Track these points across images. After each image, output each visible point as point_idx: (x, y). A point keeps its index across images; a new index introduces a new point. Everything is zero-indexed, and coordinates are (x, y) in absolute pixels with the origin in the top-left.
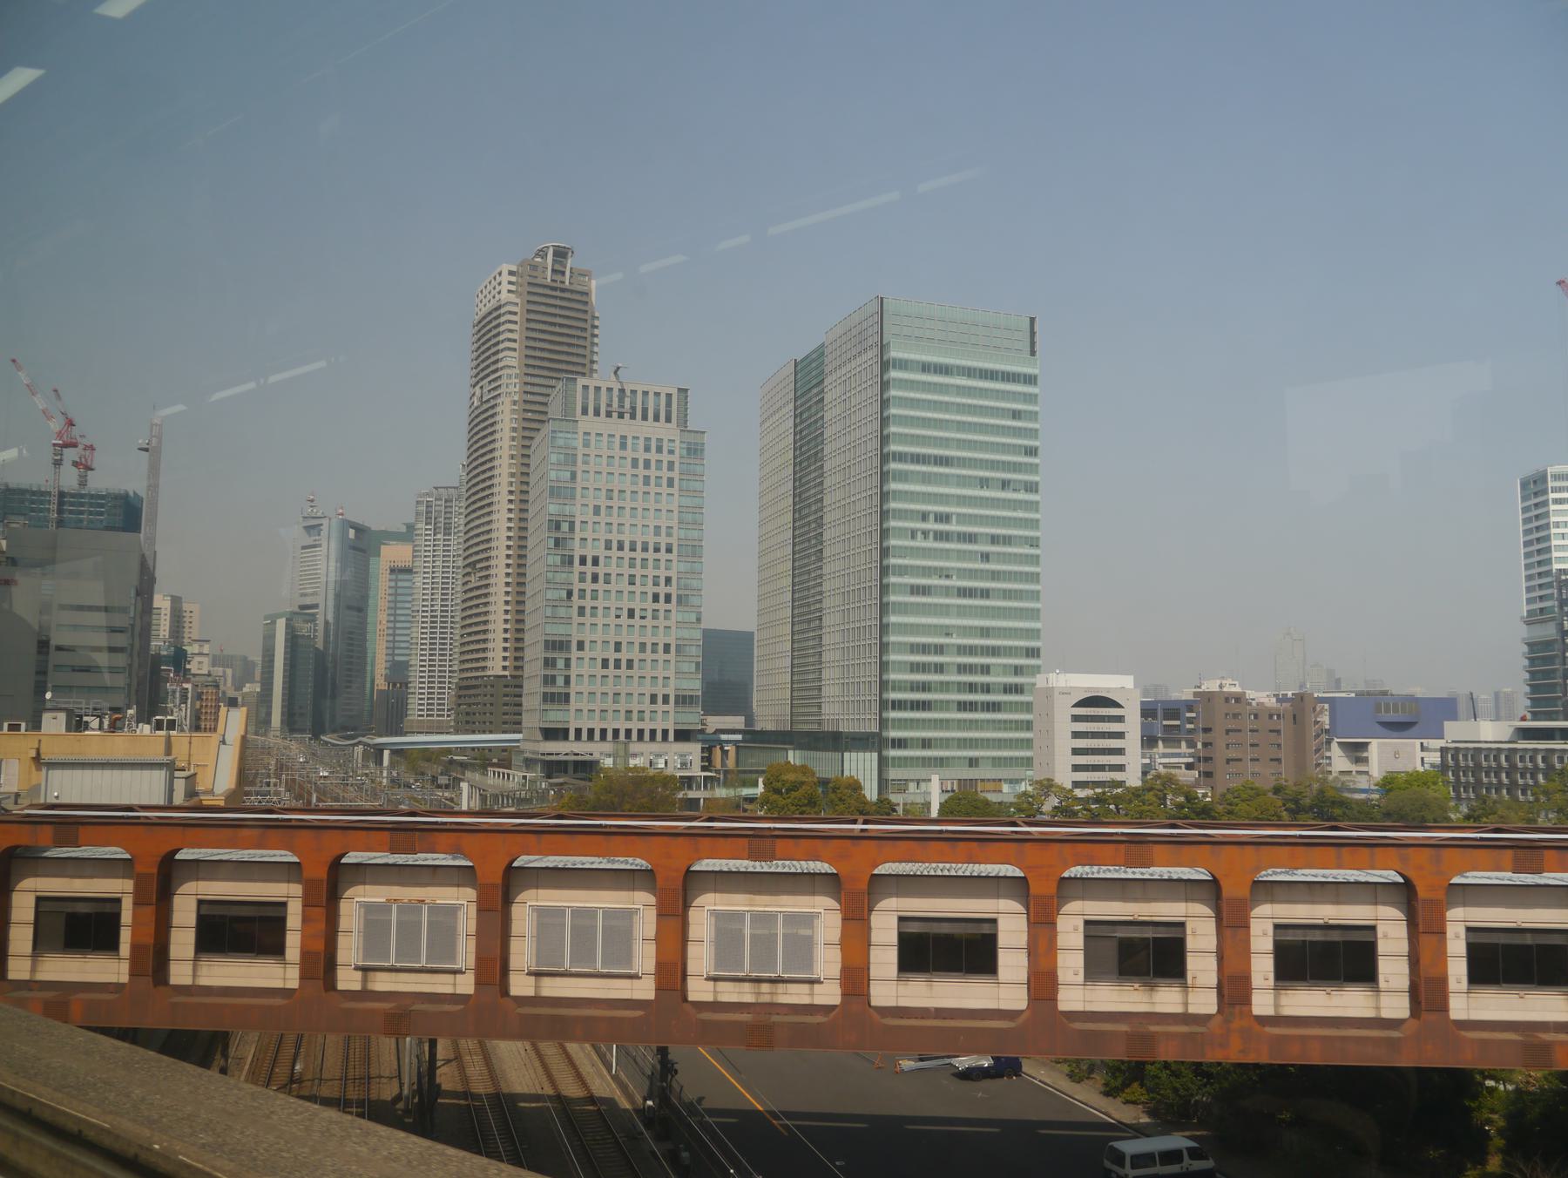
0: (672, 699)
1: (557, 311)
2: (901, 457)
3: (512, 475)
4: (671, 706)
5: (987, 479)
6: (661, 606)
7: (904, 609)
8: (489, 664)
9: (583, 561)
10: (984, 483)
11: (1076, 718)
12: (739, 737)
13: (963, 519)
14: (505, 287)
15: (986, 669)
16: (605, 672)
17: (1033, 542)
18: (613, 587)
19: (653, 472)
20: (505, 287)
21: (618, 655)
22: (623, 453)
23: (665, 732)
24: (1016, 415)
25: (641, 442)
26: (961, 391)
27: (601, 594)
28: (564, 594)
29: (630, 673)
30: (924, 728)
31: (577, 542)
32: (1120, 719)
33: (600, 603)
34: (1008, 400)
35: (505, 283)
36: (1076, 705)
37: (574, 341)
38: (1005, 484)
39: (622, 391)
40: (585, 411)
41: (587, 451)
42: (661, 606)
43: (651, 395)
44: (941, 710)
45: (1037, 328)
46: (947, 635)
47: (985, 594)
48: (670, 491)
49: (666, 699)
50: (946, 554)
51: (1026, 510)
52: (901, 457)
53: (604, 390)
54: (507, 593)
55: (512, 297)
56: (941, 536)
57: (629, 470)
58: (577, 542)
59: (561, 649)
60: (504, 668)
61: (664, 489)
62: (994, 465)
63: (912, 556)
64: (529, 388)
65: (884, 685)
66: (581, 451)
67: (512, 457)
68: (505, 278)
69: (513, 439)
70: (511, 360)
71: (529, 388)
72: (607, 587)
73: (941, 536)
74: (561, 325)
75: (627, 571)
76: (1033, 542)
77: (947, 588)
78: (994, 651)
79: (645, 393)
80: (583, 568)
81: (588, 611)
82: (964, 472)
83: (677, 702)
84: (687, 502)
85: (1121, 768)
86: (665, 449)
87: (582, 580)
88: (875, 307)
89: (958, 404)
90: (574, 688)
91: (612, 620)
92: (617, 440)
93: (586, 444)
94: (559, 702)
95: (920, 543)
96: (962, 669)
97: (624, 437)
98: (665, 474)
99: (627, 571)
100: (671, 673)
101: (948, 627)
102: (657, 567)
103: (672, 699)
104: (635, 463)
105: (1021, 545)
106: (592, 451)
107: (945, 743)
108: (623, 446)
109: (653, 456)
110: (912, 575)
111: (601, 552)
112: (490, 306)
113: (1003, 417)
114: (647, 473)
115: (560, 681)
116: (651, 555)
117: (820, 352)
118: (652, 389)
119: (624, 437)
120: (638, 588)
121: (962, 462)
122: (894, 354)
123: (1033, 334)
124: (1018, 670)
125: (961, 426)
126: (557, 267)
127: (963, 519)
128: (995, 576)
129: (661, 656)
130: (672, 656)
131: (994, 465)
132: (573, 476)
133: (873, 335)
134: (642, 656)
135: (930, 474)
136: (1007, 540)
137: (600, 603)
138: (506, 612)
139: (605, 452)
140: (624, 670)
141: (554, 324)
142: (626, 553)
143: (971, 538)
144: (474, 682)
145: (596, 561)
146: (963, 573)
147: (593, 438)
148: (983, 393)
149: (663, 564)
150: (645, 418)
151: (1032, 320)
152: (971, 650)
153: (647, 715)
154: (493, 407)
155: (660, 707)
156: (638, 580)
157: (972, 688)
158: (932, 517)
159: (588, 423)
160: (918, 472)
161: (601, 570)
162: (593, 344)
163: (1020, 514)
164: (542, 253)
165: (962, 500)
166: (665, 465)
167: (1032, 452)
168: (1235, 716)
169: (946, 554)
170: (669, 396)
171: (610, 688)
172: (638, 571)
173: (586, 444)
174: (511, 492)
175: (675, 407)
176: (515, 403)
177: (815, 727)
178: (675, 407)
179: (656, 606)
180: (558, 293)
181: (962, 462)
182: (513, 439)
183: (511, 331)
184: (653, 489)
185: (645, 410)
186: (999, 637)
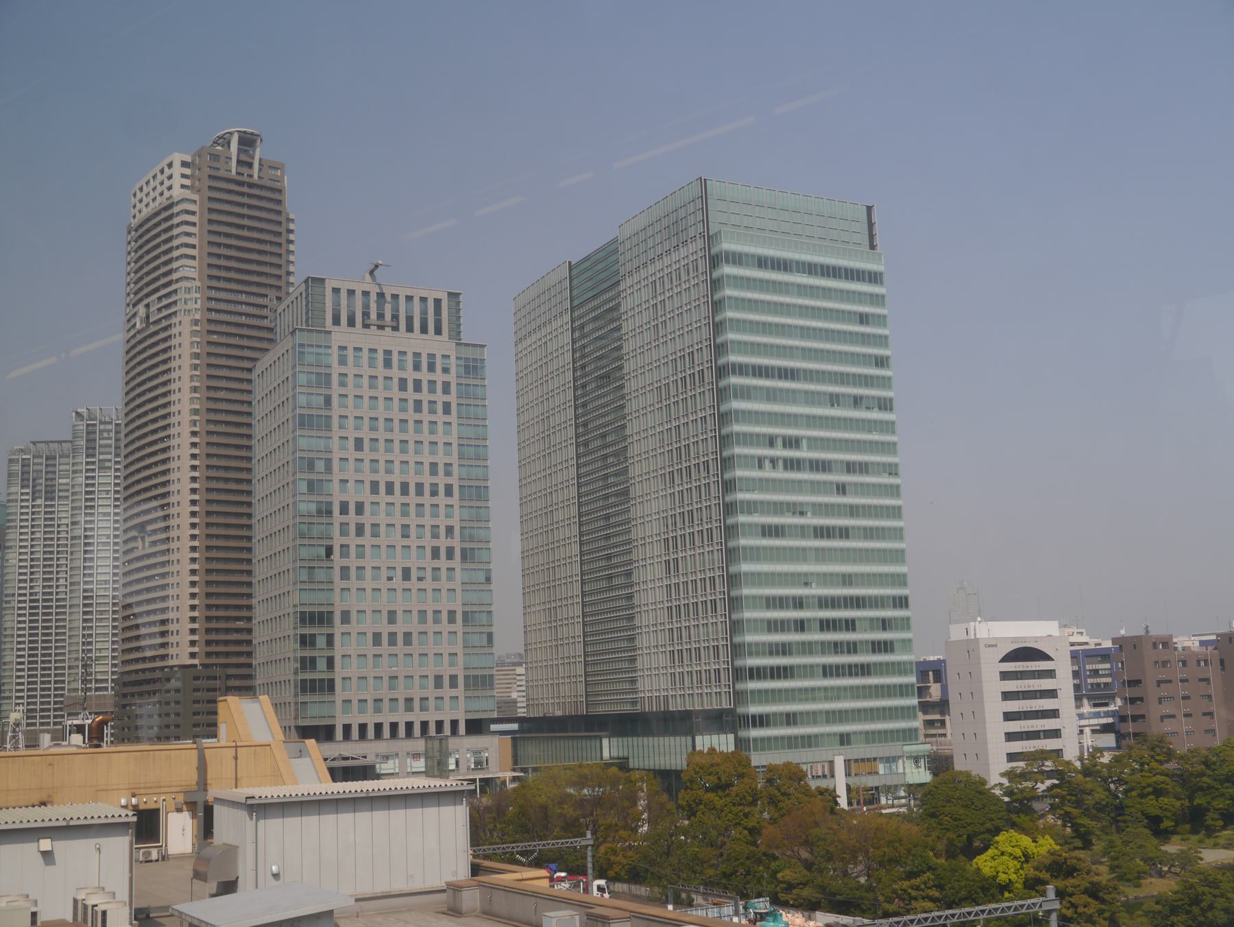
0: (461, 681)
1: (245, 211)
2: (741, 370)
3: (196, 412)
4: (460, 691)
5: (837, 395)
6: (443, 563)
7: (756, 554)
8: (171, 651)
9: (344, 509)
10: (834, 400)
11: (1005, 676)
12: (515, 726)
13: (814, 443)
14: (177, 181)
15: (850, 625)
16: (377, 650)
17: (892, 470)
18: (383, 541)
19: (425, 396)
20: (177, 181)
21: (392, 628)
22: (388, 373)
23: (454, 724)
24: (863, 319)
25: (410, 358)
26: (803, 290)
27: (368, 550)
28: (322, 552)
29: (408, 649)
30: (787, 700)
31: (336, 485)
32: (1050, 674)
33: (368, 562)
34: (854, 302)
35: (177, 177)
36: (1004, 660)
37: (267, 248)
38: (857, 401)
39: (381, 295)
40: (336, 321)
41: (343, 370)
42: (443, 563)
43: (416, 301)
44: (805, 676)
45: (875, 218)
46: (806, 584)
47: (844, 533)
48: (447, 418)
49: (453, 680)
50: (798, 486)
51: (881, 431)
52: (741, 370)
53: (358, 294)
54: (193, 560)
55: (188, 194)
56: (791, 464)
57: (396, 393)
58: (336, 485)
59: (321, 622)
60: (193, 655)
61: (440, 417)
62: (843, 379)
63: (761, 490)
64: (213, 305)
65: (737, 650)
66: (336, 370)
67: (195, 389)
68: (177, 170)
69: (195, 367)
70: (189, 272)
71: (213, 305)
72: (375, 541)
73: (791, 464)
74: (250, 228)
75: (398, 521)
76: (892, 470)
77: (802, 527)
78: (858, 602)
79: (409, 298)
80: (344, 518)
81: (353, 573)
82: (812, 387)
83: (467, 685)
84: (469, 432)
85: (1056, 734)
86: (439, 367)
87: (344, 532)
88: (696, 190)
89: (800, 307)
90: (339, 673)
91: (383, 584)
92: (380, 356)
93: (343, 361)
94: (322, 690)
95: (768, 473)
96: (826, 625)
97: (388, 353)
98: (440, 398)
99: (398, 521)
100: (458, 648)
101: (806, 574)
102: (435, 515)
103: (461, 681)
104: (403, 384)
105: (879, 474)
106: (350, 370)
107: (812, 717)
108: (388, 364)
109: (424, 376)
110: (762, 513)
111: (366, 496)
112: (154, 206)
113: (850, 322)
114: (417, 396)
115: (322, 664)
116: (427, 499)
117: (610, 251)
118: (417, 294)
119: (388, 353)
120: (413, 542)
121: (810, 376)
122: (727, 245)
123: (871, 225)
124: (885, 624)
125: (805, 332)
126: (244, 158)
127: (814, 443)
128: (853, 511)
129: (445, 627)
130: (458, 626)
131: (843, 379)
132: (328, 401)
133: (689, 226)
134: (422, 628)
135: (775, 389)
136: (863, 468)
137: (368, 562)
138: (193, 584)
139: (366, 371)
140: (400, 648)
141: (242, 227)
142: (397, 497)
143: (823, 466)
144: (148, 676)
145: (360, 508)
146: (820, 509)
147: (350, 353)
148: (827, 293)
149: (442, 510)
150: (410, 329)
151: (869, 209)
152: (832, 603)
153: (431, 703)
154: (165, 329)
155: (447, 692)
156: (413, 531)
157: (837, 647)
158: (780, 441)
159: (341, 336)
160: (761, 388)
161: (367, 519)
162: (289, 252)
163: (875, 437)
164: (225, 141)
165: (812, 421)
166: (439, 387)
167: (881, 362)
168: (1164, 664)
169: (798, 486)
170: (438, 302)
171: (384, 670)
172: (412, 520)
173: (343, 361)
174: (194, 434)
175: (442, 316)
176: (196, 322)
177: (627, 708)
178: (442, 316)
179: (436, 564)
180: (245, 189)
181: (810, 376)
182: (195, 367)
183: (188, 234)
184: (425, 417)
185: (410, 320)
186: (862, 585)
